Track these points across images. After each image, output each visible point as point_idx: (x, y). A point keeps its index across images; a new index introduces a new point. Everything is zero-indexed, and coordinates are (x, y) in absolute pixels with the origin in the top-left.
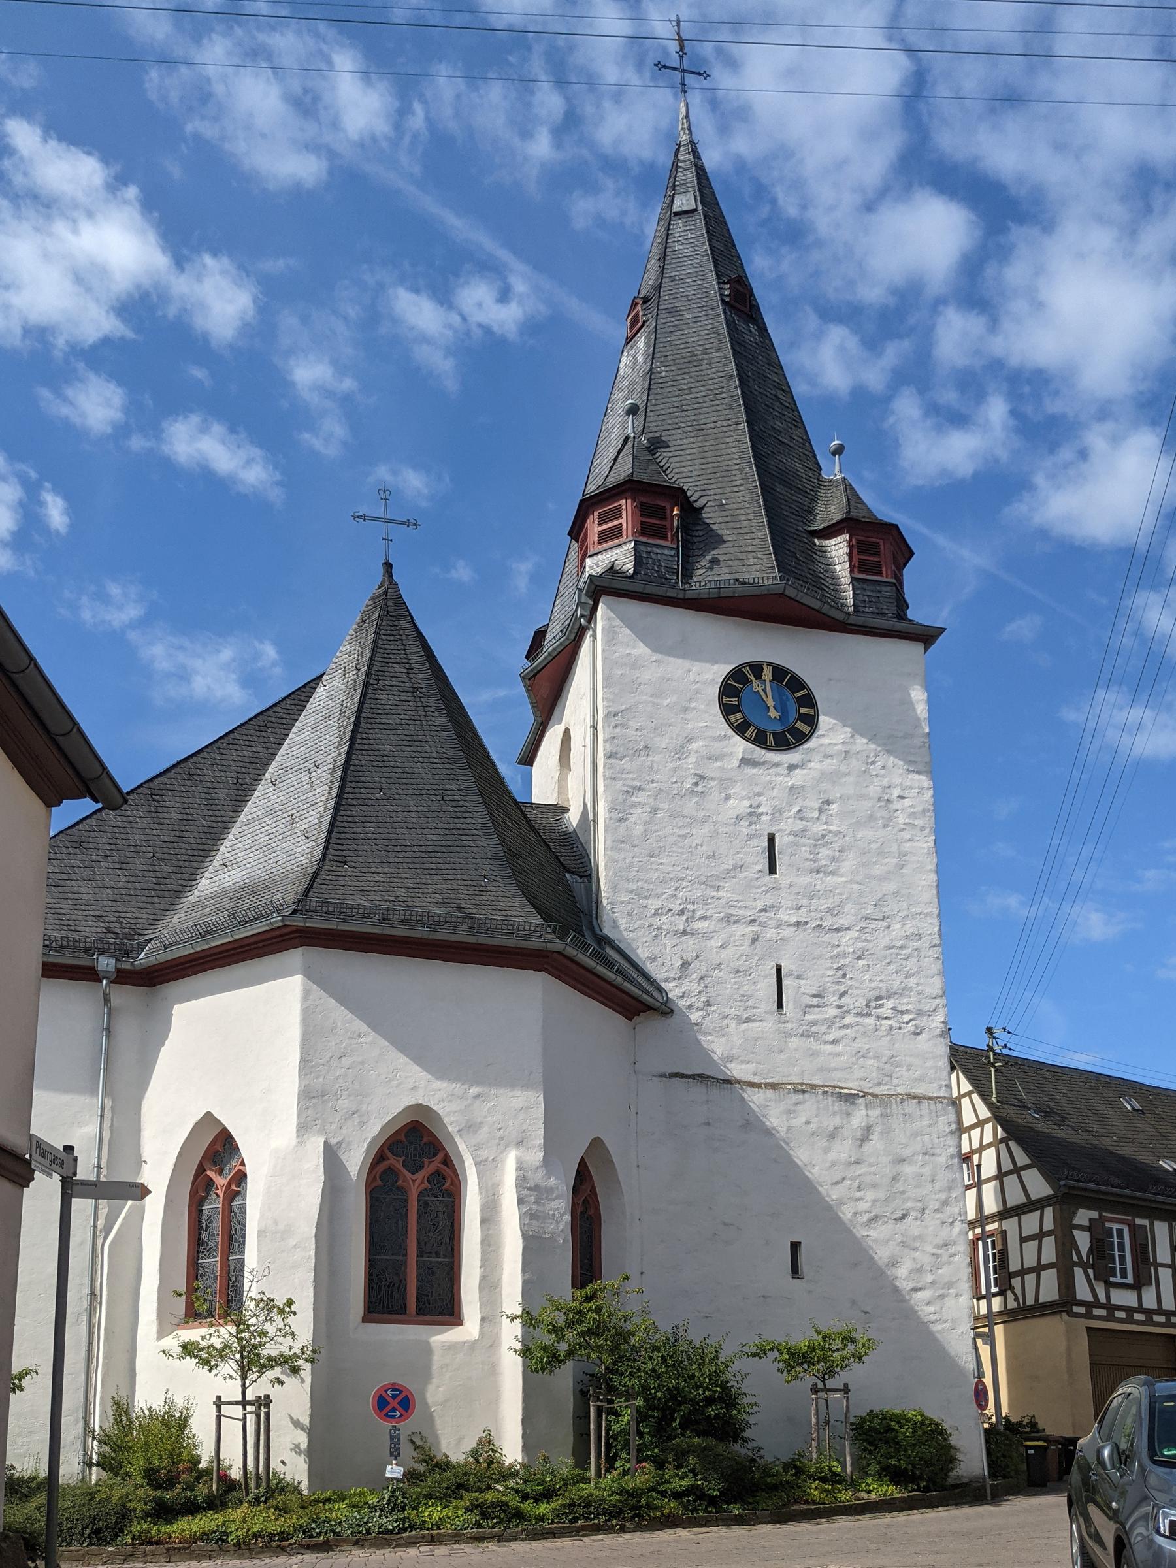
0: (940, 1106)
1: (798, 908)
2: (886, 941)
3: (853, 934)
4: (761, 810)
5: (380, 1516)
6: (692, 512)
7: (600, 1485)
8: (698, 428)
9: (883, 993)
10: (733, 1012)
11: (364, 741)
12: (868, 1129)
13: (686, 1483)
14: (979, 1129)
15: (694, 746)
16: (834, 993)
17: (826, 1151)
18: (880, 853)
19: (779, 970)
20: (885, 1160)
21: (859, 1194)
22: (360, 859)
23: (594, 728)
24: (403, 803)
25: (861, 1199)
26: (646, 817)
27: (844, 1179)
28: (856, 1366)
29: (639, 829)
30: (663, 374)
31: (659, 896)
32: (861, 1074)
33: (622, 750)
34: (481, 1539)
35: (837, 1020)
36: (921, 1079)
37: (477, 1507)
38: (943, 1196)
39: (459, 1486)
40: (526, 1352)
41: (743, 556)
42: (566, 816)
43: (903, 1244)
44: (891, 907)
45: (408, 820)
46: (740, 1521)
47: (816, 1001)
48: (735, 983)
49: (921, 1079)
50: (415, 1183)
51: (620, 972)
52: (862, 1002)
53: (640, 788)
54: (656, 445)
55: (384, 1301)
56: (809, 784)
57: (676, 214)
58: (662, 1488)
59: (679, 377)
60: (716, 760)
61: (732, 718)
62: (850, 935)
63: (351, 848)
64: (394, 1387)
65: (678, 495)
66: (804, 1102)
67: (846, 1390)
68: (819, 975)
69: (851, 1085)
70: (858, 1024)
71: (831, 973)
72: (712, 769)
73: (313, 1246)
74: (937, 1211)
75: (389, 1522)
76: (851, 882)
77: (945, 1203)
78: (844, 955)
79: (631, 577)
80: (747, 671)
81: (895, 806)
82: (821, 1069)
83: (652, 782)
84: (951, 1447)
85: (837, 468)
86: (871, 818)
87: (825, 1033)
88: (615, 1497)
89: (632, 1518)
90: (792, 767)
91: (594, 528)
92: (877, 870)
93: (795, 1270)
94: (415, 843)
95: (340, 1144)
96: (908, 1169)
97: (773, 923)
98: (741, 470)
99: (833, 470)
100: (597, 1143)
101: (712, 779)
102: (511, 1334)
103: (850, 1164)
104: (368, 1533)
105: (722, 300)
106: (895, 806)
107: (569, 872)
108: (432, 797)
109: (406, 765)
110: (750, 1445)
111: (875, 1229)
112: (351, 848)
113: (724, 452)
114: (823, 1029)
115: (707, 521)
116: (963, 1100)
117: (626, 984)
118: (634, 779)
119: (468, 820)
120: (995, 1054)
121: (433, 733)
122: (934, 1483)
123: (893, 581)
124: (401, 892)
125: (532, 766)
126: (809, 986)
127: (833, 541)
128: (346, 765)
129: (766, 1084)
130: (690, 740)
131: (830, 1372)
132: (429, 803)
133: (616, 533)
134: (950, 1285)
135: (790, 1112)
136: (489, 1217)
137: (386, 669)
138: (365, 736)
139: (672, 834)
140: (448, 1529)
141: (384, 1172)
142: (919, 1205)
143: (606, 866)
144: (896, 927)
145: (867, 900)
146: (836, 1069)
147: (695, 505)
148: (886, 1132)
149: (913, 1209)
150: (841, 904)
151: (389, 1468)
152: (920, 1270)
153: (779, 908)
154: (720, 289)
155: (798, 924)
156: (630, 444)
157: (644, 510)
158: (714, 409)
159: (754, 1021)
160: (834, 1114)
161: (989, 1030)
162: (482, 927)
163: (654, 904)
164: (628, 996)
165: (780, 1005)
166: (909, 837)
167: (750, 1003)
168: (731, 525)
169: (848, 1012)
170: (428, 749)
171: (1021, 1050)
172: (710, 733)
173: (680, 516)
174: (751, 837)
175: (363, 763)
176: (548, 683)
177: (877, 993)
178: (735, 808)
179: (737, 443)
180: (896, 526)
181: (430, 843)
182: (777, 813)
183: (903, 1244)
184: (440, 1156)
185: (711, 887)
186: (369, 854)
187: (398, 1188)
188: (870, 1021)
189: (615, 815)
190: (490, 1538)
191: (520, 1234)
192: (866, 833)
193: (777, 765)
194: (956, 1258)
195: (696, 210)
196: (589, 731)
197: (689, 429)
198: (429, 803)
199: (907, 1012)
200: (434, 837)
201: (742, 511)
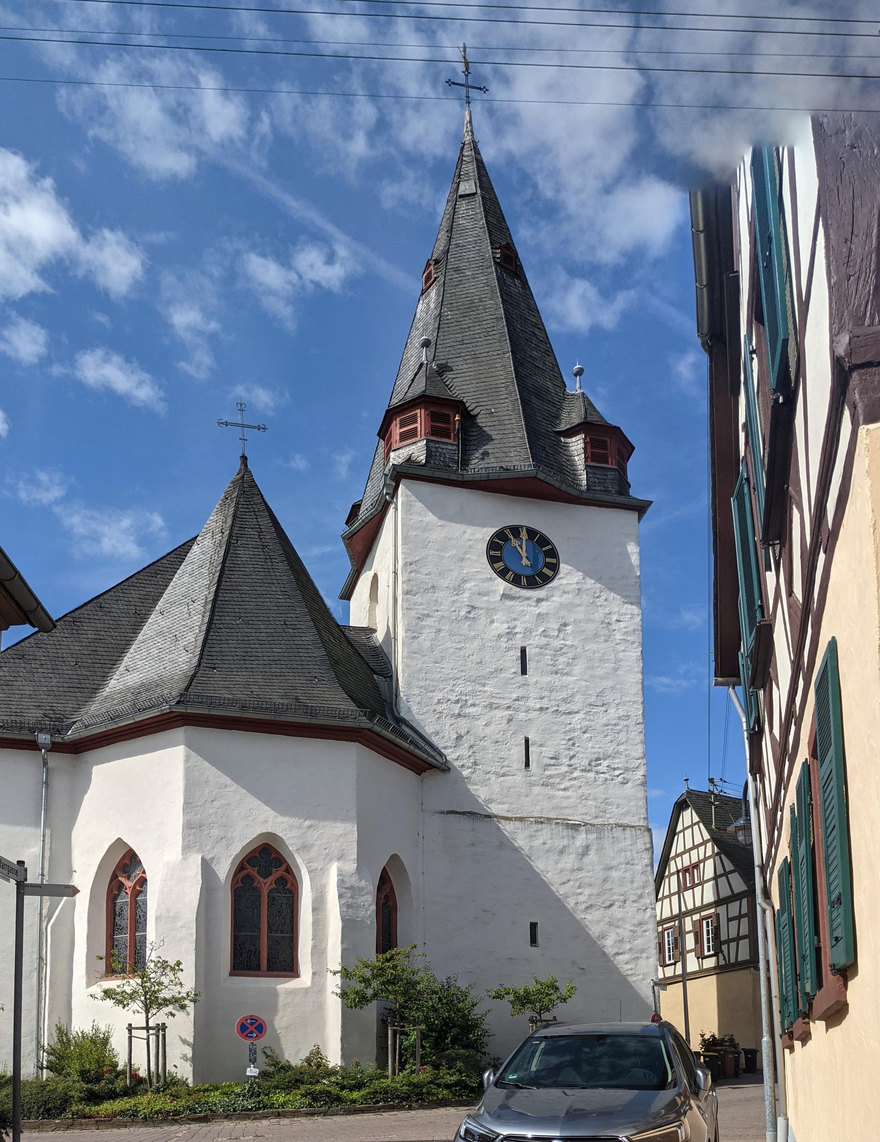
1: (542, 698)
2: (604, 721)
3: (581, 716)
4: (516, 630)
6: (469, 418)
8: (475, 357)
9: (601, 756)
10: (493, 769)
12: (587, 848)
13: (454, 1078)
15: (468, 585)
17: (557, 862)
18: (602, 660)
19: (527, 741)
20: (598, 868)
21: (579, 891)
22: (225, 666)
23: (395, 573)
24: (256, 627)
25: (580, 894)
26: (432, 635)
29: (427, 644)
31: (441, 690)
34: (312, 1114)
36: (625, 814)
37: (309, 1094)
38: (639, 892)
39: (297, 1081)
40: (344, 995)
41: (507, 450)
42: (375, 635)
43: (610, 924)
45: (260, 638)
49: (625, 814)
50: (266, 885)
51: (412, 742)
52: (585, 762)
53: (428, 616)
54: (443, 369)
55: (245, 961)
57: (461, 196)
58: (438, 1082)
61: (496, 566)
65: (459, 406)
66: (542, 830)
68: (557, 744)
69: (576, 818)
71: (564, 742)
72: (481, 602)
74: (635, 901)
75: (249, 1104)
76: (580, 680)
77: (641, 897)
78: (574, 730)
79: (424, 465)
80: (508, 532)
82: (556, 808)
83: (437, 611)
85: (578, 385)
86: (596, 635)
88: (405, 1088)
90: (539, 601)
91: (396, 430)
92: (599, 672)
93: (534, 941)
94: (265, 654)
95: (212, 859)
96: (615, 874)
98: (506, 387)
99: (574, 387)
100: (394, 858)
102: (333, 983)
104: (235, 1110)
105: (495, 261)
107: (376, 674)
109: (259, 600)
113: (494, 374)
114: (558, 780)
115: (481, 425)
117: (416, 750)
118: (424, 609)
119: (303, 638)
124: (255, 688)
126: (548, 751)
127: (574, 439)
128: (215, 601)
129: (516, 818)
130: (465, 581)
133: (413, 434)
134: (642, 951)
135: (531, 836)
136: (318, 906)
145: (590, 692)
148: (600, 850)
149: (618, 900)
150: (573, 695)
151: (248, 1069)
152: (622, 941)
153: (528, 698)
154: (493, 253)
156: (424, 369)
157: (434, 417)
160: (563, 837)
163: (438, 695)
164: (419, 759)
165: (527, 765)
167: (506, 763)
168: (498, 427)
169: (575, 769)
170: (274, 589)
172: (479, 576)
173: (460, 421)
174: (508, 649)
176: (362, 542)
177: (596, 756)
178: (497, 629)
179: (504, 366)
181: (276, 654)
182: (528, 632)
184: (284, 867)
186: (232, 662)
188: (591, 775)
189: (410, 634)
192: (592, 646)
193: (528, 599)
195: (476, 193)
196: (392, 576)
199: (618, 768)
201: (507, 417)
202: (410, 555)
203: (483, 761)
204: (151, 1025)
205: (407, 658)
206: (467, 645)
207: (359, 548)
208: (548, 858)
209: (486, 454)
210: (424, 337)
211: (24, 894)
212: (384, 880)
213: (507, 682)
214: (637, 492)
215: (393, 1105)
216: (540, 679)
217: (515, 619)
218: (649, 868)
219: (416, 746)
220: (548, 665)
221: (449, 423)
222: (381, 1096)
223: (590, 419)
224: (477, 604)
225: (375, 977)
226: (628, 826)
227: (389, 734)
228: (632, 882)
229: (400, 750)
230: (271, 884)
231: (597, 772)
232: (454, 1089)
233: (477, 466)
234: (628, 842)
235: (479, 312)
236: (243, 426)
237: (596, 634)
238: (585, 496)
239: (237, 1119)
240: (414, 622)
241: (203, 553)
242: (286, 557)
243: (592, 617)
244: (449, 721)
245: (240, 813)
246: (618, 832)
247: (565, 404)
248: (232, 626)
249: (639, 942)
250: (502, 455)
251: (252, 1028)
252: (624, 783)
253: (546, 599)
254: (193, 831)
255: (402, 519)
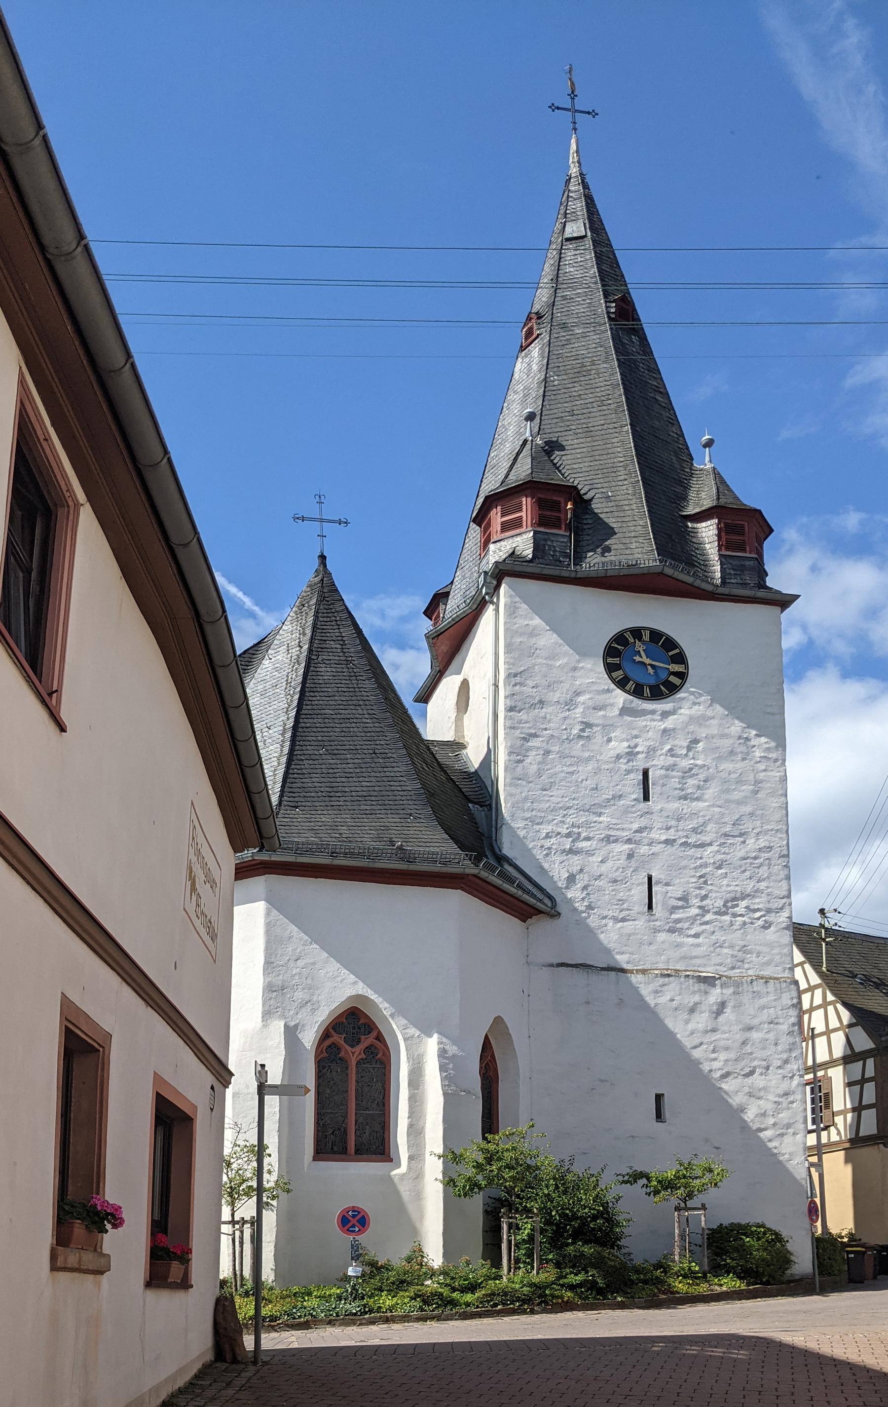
0: (784, 985)
1: (668, 829)
2: (742, 854)
3: (714, 848)
4: (637, 750)
5: (345, 1303)
6: (583, 504)
7: (511, 1279)
8: (588, 431)
9: (738, 895)
10: (611, 913)
11: (309, 707)
12: (722, 1005)
13: (580, 1278)
14: (810, 993)
15: (581, 699)
16: (696, 896)
17: (687, 1022)
18: (739, 782)
19: (650, 879)
20: (735, 1028)
21: (713, 1056)
22: (309, 804)
25: (715, 1059)
26: (539, 758)
27: (701, 1044)
28: (713, 1191)
29: (535, 767)
30: (556, 383)
31: (549, 822)
32: (717, 960)
33: (522, 697)
34: (424, 1319)
35: (699, 918)
36: (768, 963)
37: (419, 1296)
38: (785, 1056)
39: (402, 1282)
40: (449, 1182)
41: (628, 541)
42: (464, 752)
43: (750, 1094)
44: (747, 826)
45: (346, 770)
46: (622, 1306)
47: (680, 903)
48: (613, 890)
49: (768, 963)
50: (354, 1054)
51: (520, 886)
52: (719, 903)
53: (535, 736)
54: (552, 447)
55: (331, 1143)
56: (679, 727)
57: (568, 240)
58: (561, 1282)
59: (570, 386)
60: (600, 709)
61: (614, 675)
62: (710, 849)
63: (301, 795)
64: (354, 1209)
65: (572, 493)
66: (669, 984)
67: (704, 1207)
68: (683, 883)
69: (709, 969)
70: (716, 920)
71: (694, 880)
72: (597, 717)
73: (278, 1104)
74: (779, 1067)
75: (353, 1307)
77: (786, 1062)
78: (705, 865)
79: (531, 561)
81: (752, 743)
82: (684, 958)
83: (546, 729)
84: (788, 1252)
85: (707, 459)
86: (732, 753)
87: (688, 929)
89: (539, 1304)
90: (665, 715)
91: (496, 517)
92: (736, 795)
93: (659, 1116)
94: (353, 789)
95: (296, 1026)
96: (755, 1035)
97: (646, 841)
98: (625, 467)
99: (704, 462)
100: (498, 1020)
101: (597, 725)
102: (433, 1169)
103: (707, 1032)
104: (337, 1315)
105: (609, 317)
106: (752, 743)
107: (472, 802)
108: (365, 751)
109: (344, 725)
110: (624, 1251)
111: (727, 1082)
112: (301, 795)
113: (610, 451)
114: (686, 925)
115: (596, 511)
116: (796, 969)
117: (525, 895)
118: (530, 728)
119: (396, 769)
120: (827, 929)
121: (364, 698)
122: (774, 1278)
123: (756, 556)
124: (343, 830)
125: (427, 703)
126: (676, 891)
127: (704, 524)
128: (295, 728)
129: (637, 971)
130: (578, 694)
131: (690, 1195)
132: (364, 756)
133: (517, 524)
134: (788, 1126)
135: (657, 992)
136: (416, 1080)
137: (324, 646)
138: (308, 703)
139: (562, 772)
140: (400, 1313)
141: (330, 1046)
142: (764, 1063)
143: (505, 799)
144: (751, 841)
145: (726, 820)
146: (696, 957)
147: (585, 497)
148: (738, 1006)
149: (759, 1066)
150: (704, 824)
151: (350, 1269)
152: (764, 1115)
153: (651, 829)
154: (607, 307)
155: (667, 842)
156: (528, 446)
157: (541, 504)
158: (601, 413)
159: (628, 920)
160: (694, 993)
161: (822, 911)
162: (409, 858)
163: (546, 829)
164: (524, 901)
165: (650, 907)
166: (764, 767)
167: (625, 906)
168: (616, 514)
169: (708, 911)
170: (360, 712)
171: (847, 924)
172: (595, 688)
173: (574, 510)
174: (628, 772)
175: (308, 725)
176: (450, 644)
177: (733, 895)
178: (615, 748)
179: (623, 442)
180: (760, 511)
181: (364, 789)
182: (651, 752)
183: (750, 1094)
184: (374, 1034)
185: (594, 813)
186: (316, 799)
187: (340, 1059)
188: (727, 918)
189: (514, 757)
190: (432, 1318)
191: (441, 1092)
192: (727, 766)
193: (653, 712)
194: (794, 1105)
195: (585, 236)
196: (492, 688)
197: (578, 431)
198: (364, 756)
199: (758, 910)
200: (368, 784)
201: (626, 502)
202: (513, 664)
203: (599, 903)
204: (237, 1218)
205: (511, 785)
206: (580, 768)
207: (444, 646)
208: (676, 1017)
209: (608, 549)
210: (529, 410)
211: (264, 1094)
212: (487, 1045)
213: (626, 811)
214: (778, 579)
215: (513, 1308)
216: (666, 806)
217: (636, 737)
218: (796, 1028)
219: (533, 896)
220: (676, 789)
221: (559, 511)
222: (499, 1298)
223: (722, 501)
224: (592, 720)
225: (489, 1161)
226: (771, 978)
227: (513, 890)
228: (776, 1044)
229: (505, 896)
230: (360, 1054)
231: (735, 915)
232: (579, 1290)
233: (593, 561)
234: (772, 997)
235: (591, 377)
236: (322, 520)
237: (732, 751)
238: (721, 590)
239: (340, 1325)
240: (519, 743)
241: (277, 669)
242: (373, 673)
243: (726, 731)
244: (558, 858)
245: (327, 973)
246: (758, 986)
247: (694, 481)
248: (314, 757)
249: (784, 1116)
250: (621, 546)
251: (354, 1221)
252: (767, 926)
253: (673, 712)
254: (275, 993)
255: (505, 623)
